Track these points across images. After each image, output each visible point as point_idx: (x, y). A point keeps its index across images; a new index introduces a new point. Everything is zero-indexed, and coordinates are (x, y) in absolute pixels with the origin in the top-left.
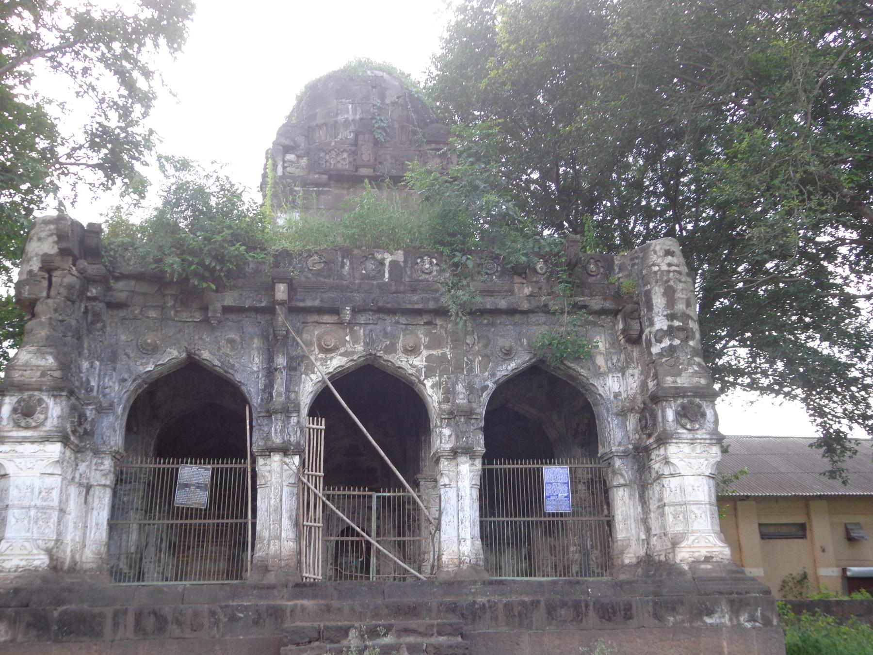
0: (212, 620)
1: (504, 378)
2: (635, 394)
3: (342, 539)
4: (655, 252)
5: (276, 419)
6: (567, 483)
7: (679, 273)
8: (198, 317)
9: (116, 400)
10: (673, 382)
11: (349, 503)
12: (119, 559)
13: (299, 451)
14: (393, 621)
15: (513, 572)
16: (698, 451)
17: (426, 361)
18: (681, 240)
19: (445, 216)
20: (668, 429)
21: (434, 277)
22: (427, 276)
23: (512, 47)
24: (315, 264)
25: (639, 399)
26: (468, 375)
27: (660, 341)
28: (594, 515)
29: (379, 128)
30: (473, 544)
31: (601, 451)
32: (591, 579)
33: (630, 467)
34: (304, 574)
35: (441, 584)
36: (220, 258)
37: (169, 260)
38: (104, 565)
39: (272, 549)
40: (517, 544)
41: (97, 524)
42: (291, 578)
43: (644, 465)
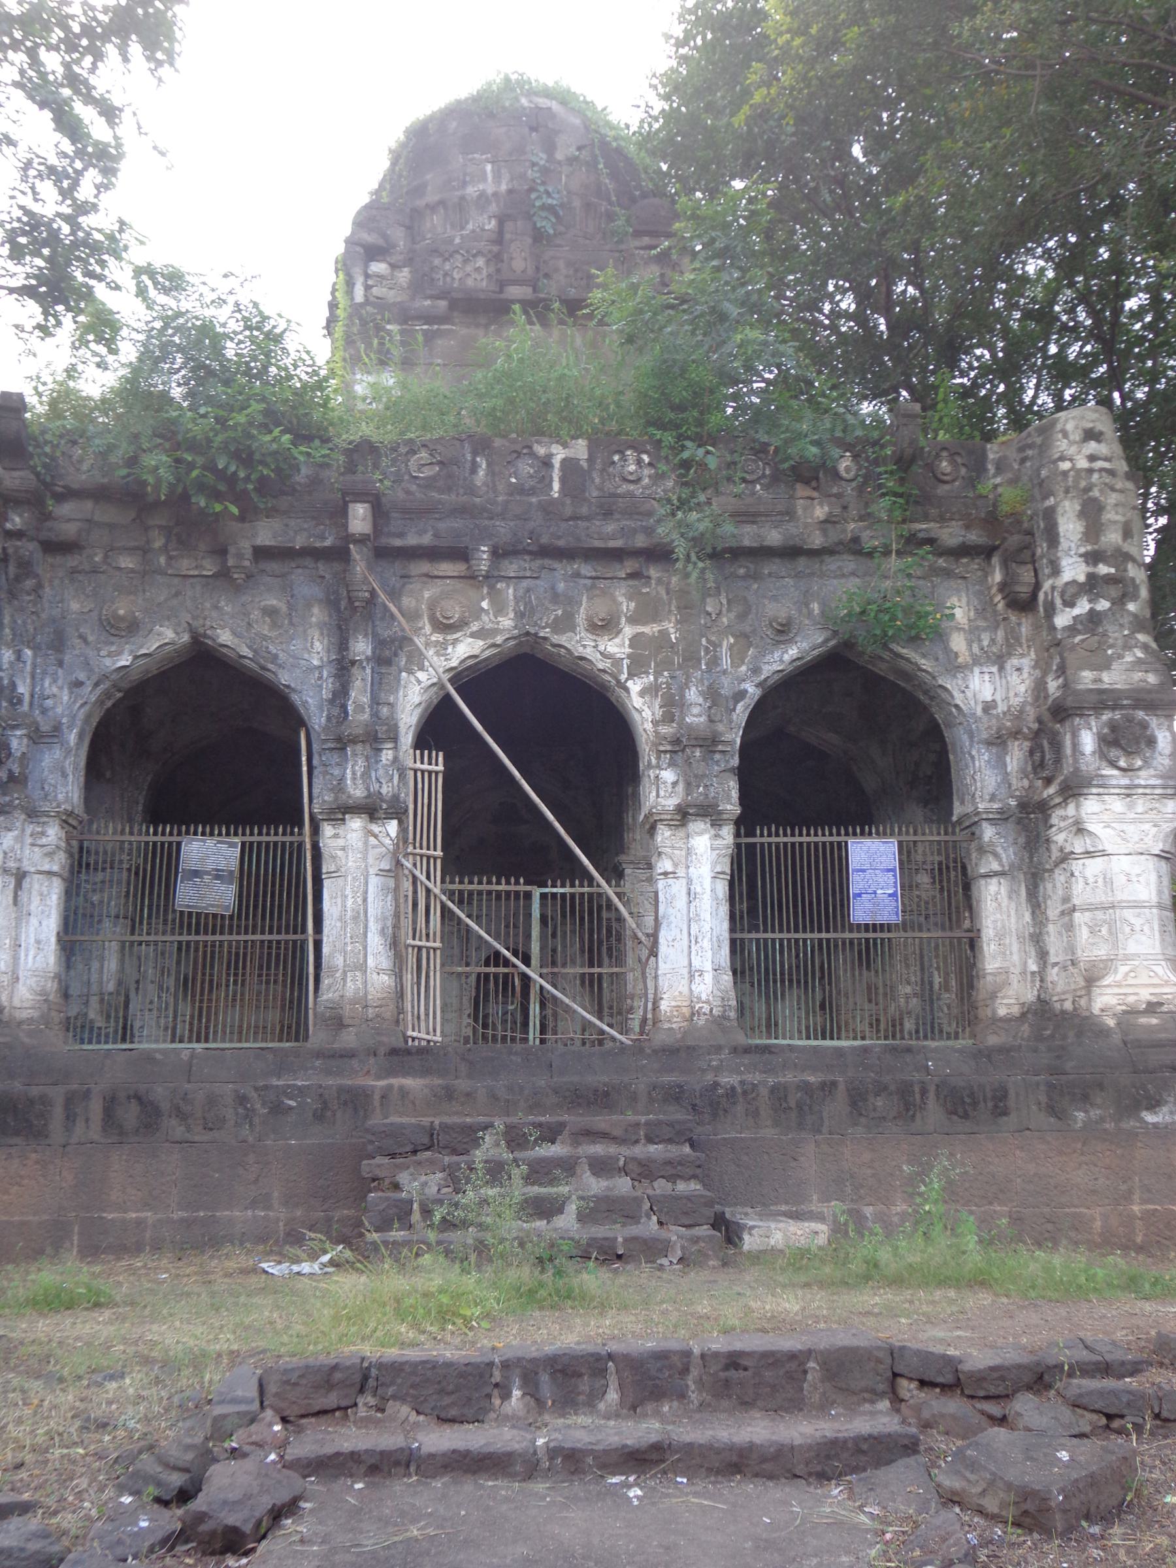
0: (241, 1111)
1: (776, 677)
2: (1024, 703)
3: (488, 970)
4: (1065, 434)
5: (355, 755)
6: (893, 870)
7: (1112, 473)
8: (209, 567)
9: (64, 720)
10: (1095, 681)
11: (498, 908)
12: (86, 1003)
13: (397, 812)
14: (566, 1117)
15: (800, 1032)
16: (1140, 809)
17: (630, 646)
18: (1122, 418)
19: (667, 372)
20: (1084, 768)
21: (644, 488)
22: (632, 487)
23: (797, 42)
24: (421, 466)
25: (1031, 713)
26: (709, 670)
27: (1070, 604)
28: (943, 929)
29: (544, 207)
30: (716, 980)
31: (958, 810)
32: (933, 1044)
33: (1011, 839)
34: (410, 1033)
35: (655, 1052)
36: (245, 457)
37: (150, 460)
38: (54, 1014)
39: (351, 987)
40: (806, 982)
41: (38, 942)
42: (385, 1039)
43: (1038, 836)
